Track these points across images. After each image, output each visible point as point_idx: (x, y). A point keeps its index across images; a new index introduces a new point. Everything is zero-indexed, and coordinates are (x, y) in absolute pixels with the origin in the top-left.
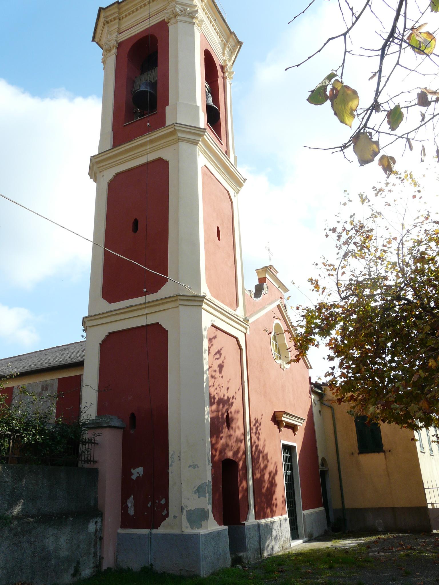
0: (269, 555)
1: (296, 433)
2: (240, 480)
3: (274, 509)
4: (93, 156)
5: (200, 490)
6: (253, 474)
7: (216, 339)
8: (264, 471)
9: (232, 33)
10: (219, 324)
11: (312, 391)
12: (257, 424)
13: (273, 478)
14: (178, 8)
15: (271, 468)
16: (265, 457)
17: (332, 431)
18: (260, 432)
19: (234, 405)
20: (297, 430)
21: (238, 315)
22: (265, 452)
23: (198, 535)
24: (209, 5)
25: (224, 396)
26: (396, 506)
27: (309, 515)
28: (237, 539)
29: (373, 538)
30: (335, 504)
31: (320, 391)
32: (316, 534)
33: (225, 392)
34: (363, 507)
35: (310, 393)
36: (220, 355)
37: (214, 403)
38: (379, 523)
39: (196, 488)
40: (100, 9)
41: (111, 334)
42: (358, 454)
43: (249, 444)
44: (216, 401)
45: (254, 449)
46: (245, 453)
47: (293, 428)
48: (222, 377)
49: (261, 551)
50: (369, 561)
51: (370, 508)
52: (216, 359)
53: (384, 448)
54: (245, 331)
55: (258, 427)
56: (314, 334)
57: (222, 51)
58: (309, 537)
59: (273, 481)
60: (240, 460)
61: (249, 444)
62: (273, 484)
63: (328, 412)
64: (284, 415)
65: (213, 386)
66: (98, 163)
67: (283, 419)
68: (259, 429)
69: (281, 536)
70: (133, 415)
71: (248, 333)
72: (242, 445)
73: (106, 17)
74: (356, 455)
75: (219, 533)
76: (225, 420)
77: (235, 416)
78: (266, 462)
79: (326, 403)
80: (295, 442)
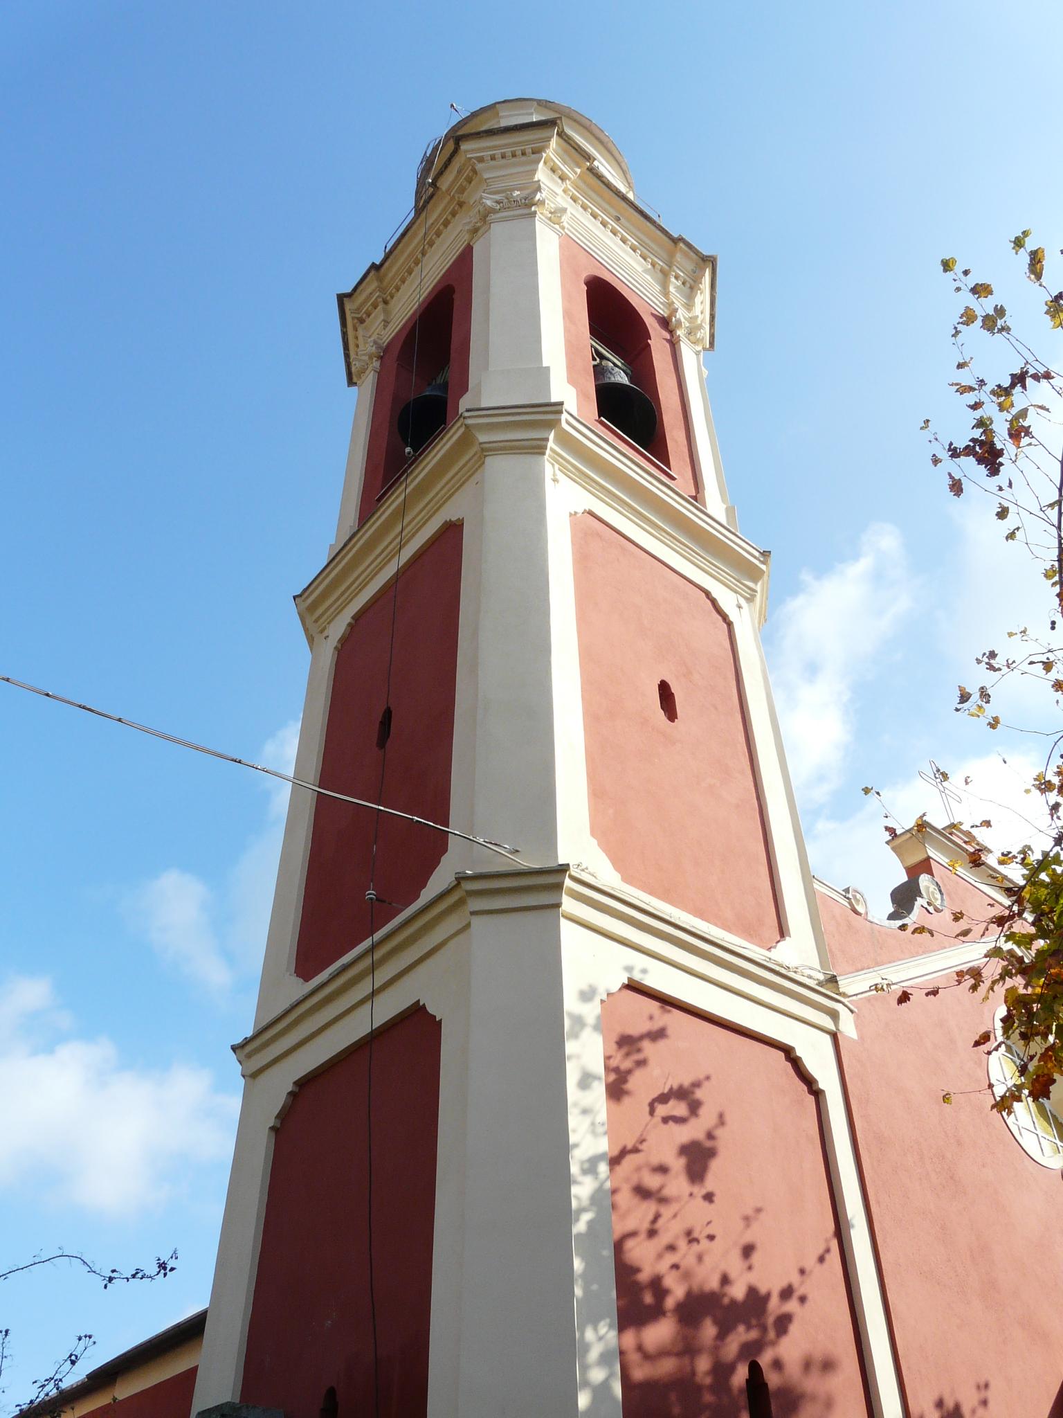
4: (300, 596)
7: (662, 1044)
9: (676, 241)
10: (661, 979)
14: (487, 198)
19: (794, 1328)
21: (786, 963)
24: (588, 185)
25: (725, 1280)
33: (734, 1264)
36: (694, 1107)
37: (656, 1312)
40: (341, 298)
41: (304, 1084)
44: (670, 1303)
48: (709, 1197)
52: (665, 1120)
54: (830, 1025)
57: (658, 288)
65: (652, 1233)
66: (312, 608)
70: (331, 1393)
71: (848, 1027)
73: (358, 310)
76: (743, 1401)
77: (812, 1384)
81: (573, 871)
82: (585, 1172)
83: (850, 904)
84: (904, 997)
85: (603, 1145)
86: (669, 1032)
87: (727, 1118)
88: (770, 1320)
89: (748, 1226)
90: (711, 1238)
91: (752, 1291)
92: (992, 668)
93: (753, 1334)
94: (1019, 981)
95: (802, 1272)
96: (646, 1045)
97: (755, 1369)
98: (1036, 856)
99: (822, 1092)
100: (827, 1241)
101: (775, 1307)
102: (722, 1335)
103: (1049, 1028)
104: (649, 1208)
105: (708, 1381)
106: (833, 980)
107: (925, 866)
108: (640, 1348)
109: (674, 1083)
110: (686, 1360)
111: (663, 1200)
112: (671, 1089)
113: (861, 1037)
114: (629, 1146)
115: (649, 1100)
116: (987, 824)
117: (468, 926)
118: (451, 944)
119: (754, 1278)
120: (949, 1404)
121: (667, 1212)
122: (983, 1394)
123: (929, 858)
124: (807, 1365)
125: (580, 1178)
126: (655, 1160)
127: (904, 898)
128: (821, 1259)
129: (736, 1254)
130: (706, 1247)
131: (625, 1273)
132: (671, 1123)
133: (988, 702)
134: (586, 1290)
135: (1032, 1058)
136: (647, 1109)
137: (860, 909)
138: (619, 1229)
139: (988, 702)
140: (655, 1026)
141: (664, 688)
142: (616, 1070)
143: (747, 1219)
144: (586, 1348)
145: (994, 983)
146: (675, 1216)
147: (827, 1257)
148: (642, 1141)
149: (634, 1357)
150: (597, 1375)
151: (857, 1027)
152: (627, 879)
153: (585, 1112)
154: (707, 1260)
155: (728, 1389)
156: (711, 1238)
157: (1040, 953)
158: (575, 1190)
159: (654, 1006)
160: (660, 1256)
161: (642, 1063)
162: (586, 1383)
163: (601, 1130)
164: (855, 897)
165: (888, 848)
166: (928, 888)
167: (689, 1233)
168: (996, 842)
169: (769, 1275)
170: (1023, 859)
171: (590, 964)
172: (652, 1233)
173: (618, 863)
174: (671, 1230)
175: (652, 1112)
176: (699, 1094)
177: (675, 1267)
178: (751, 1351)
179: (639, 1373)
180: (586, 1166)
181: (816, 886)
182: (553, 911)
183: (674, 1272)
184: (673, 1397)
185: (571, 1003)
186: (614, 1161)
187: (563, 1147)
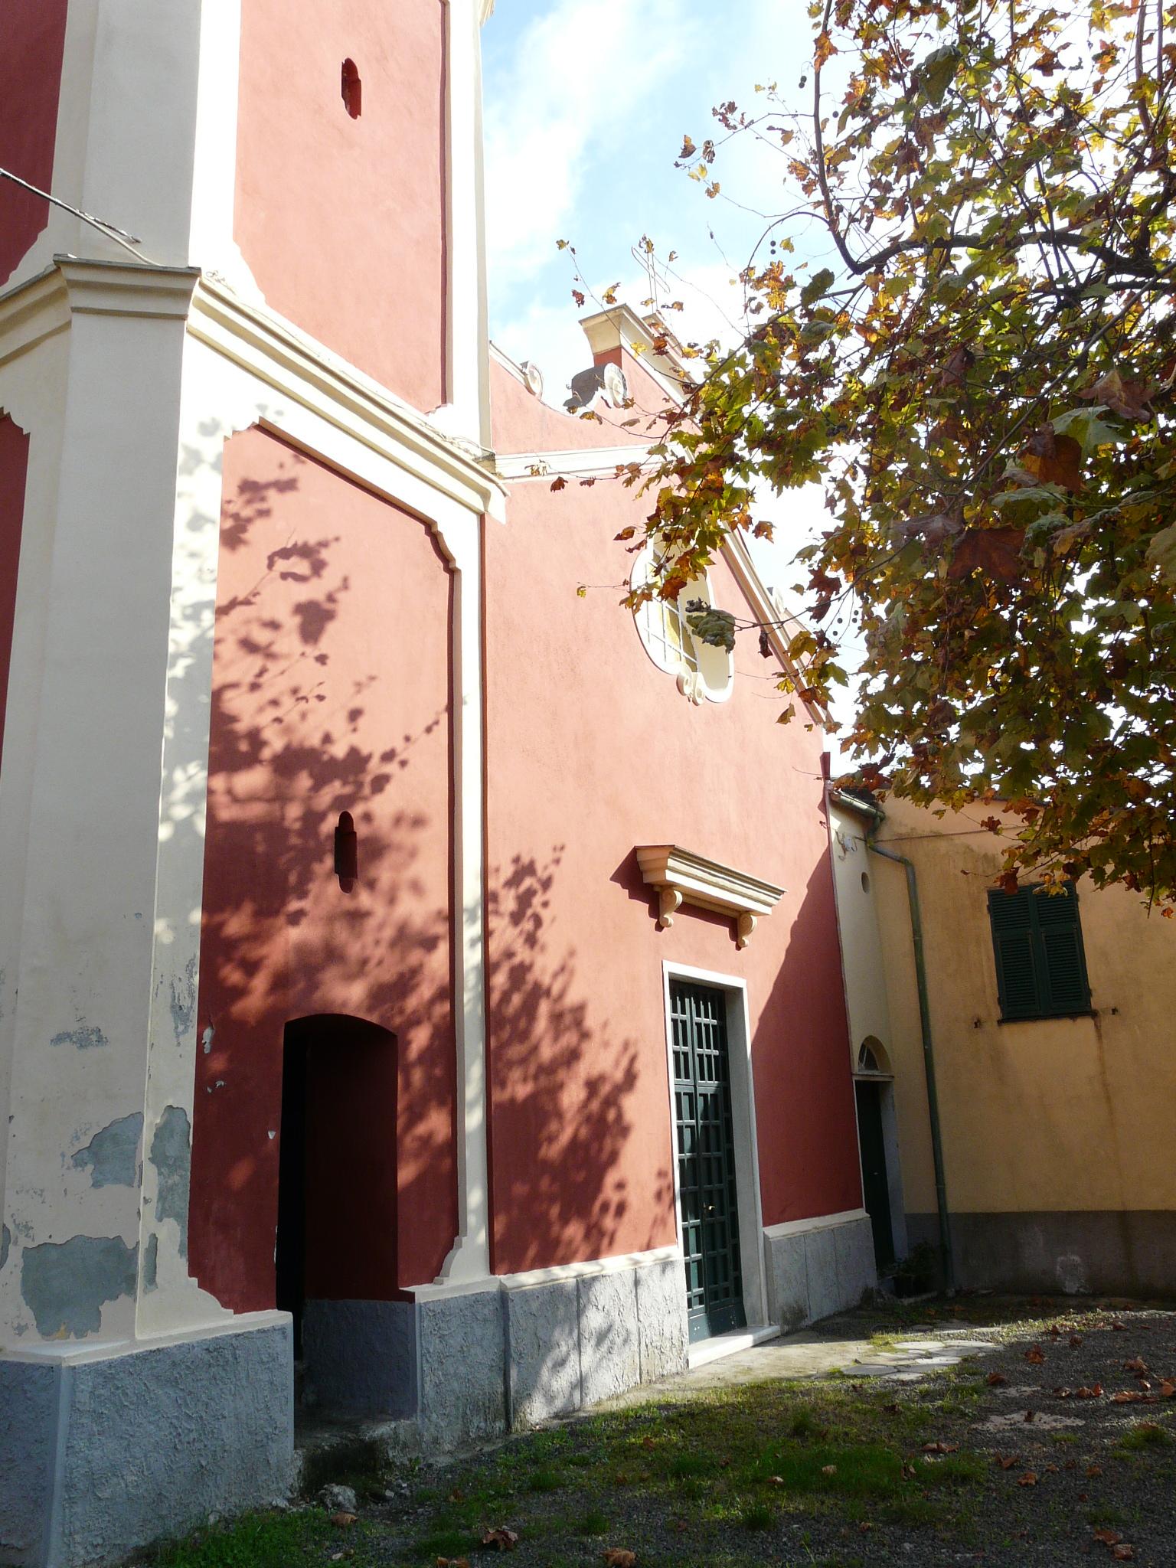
0: (556, 1416)
1: (746, 939)
2: (410, 1108)
3: (609, 1222)
5: (107, 1153)
6: (493, 1078)
7: (290, 496)
8: (562, 1074)
11: (831, 802)
12: (528, 882)
13: (612, 1101)
15: (600, 1060)
16: (568, 1019)
17: (908, 945)
18: (546, 915)
19: (389, 788)
20: (748, 929)
22: (572, 998)
23: (51, 1370)
25: (327, 739)
26: (1134, 1206)
27: (792, 1240)
28: (347, 1367)
29: (1029, 1330)
30: (912, 1194)
31: (864, 806)
32: (820, 1307)
34: (1015, 1209)
35: (823, 807)
36: (318, 567)
37: (251, 760)
38: (1069, 1265)
39: (86, 1142)
42: (1000, 1022)
43: (472, 957)
44: (266, 753)
45: (500, 979)
46: (450, 992)
47: (735, 921)
49: (508, 1407)
50: (965, 1479)
51: (1036, 1213)
52: (284, 576)
53: (1095, 1002)
54: (479, 505)
55: (530, 893)
56: (744, 468)
58: (786, 1321)
59: (611, 1115)
60: (415, 1021)
61: (472, 957)
62: (605, 1128)
63: (893, 881)
64: (671, 862)
65: (255, 687)
67: (670, 876)
68: (537, 901)
69: (636, 1329)
71: (497, 509)
72: (438, 959)
74: (991, 1026)
75: (219, 1354)
76: (330, 845)
77: (402, 836)
78: (569, 1039)
79: (887, 848)
80: (739, 973)
81: (205, 278)
82: (186, 618)
83: (526, 380)
84: (559, 485)
85: (210, 593)
86: (300, 485)
87: (352, 583)
88: (368, 779)
89: (358, 692)
90: (321, 698)
91: (354, 752)
92: (725, 120)
93: (348, 790)
94: (675, 479)
95: (407, 739)
96: (272, 494)
97: (346, 819)
98: (722, 354)
99: (459, 571)
100: (438, 713)
101: (375, 767)
102: (317, 787)
103: (692, 532)
104: (256, 662)
105: (297, 826)
106: (491, 458)
107: (614, 355)
108: (229, 792)
109: (299, 538)
110: (276, 806)
111: (270, 656)
112: (295, 545)
113: (510, 523)
114: (241, 598)
115: (269, 553)
116: (679, 306)
117: (68, 325)
118: (49, 344)
119: (356, 740)
120: (525, 860)
121: (274, 667)
122: (557, 855)
123: (620, 347)
124: (398, 820)
125: (181, 623)
126: (267, 616)
127: (585, 385)
128: (429, 730)
129: (341, 718)
130: (311, 701)
131: (221, 722)
132: (290, 580)
133: (711, 161)
134: (177, 730)
135: (668, 559)
136: (266, 562)
137: (535, 387)
138: (219, 678)
139: (711, 161)
140: (284, 476)
141: (349, 72)
142: (236, 516)
143: (359, 685)
144: (171, 786)
145: (651, 480)
146: (282, 673)
147: (435, 728)
148: (255, 594)
149: (221, 799)
150: (181, 812)
151: (507, 512)
152: (273, 302)
153: (193, 555)
154: (311, 718)
155: (316, 834)
156: (321, 698)
157: (702, 457)
158: (173, 634)
159: (288, 452)
160: (261, 710)
161: (264, 513)
162: (168, 818)
163: (208, 577)
164: (532, 373)
165: (581, 328)
166: (612, 380)
167: (295, 691)
168: (683, 328)
169: (371, 740)
170: (709, 355)
171: (215, 395)
172: (255, 687)
173: (265, 281)
174: (276, 685)
175: (271, 565)
176: (325, 554)
177: (278, 720)
178: (342, 804)
179: (226, 814)
180: (189, 611)
181: (492, 352)
182: (177, 323)
183: (276, 725)
184: (259, 837)
185: (188, 435)
186: (222, 611)
187: (163, 589)
